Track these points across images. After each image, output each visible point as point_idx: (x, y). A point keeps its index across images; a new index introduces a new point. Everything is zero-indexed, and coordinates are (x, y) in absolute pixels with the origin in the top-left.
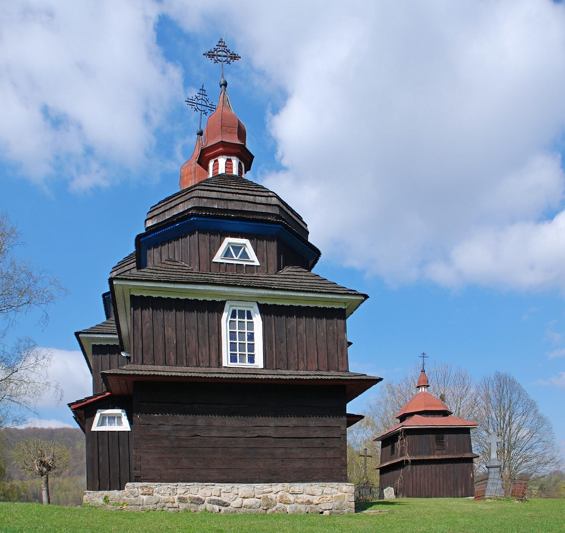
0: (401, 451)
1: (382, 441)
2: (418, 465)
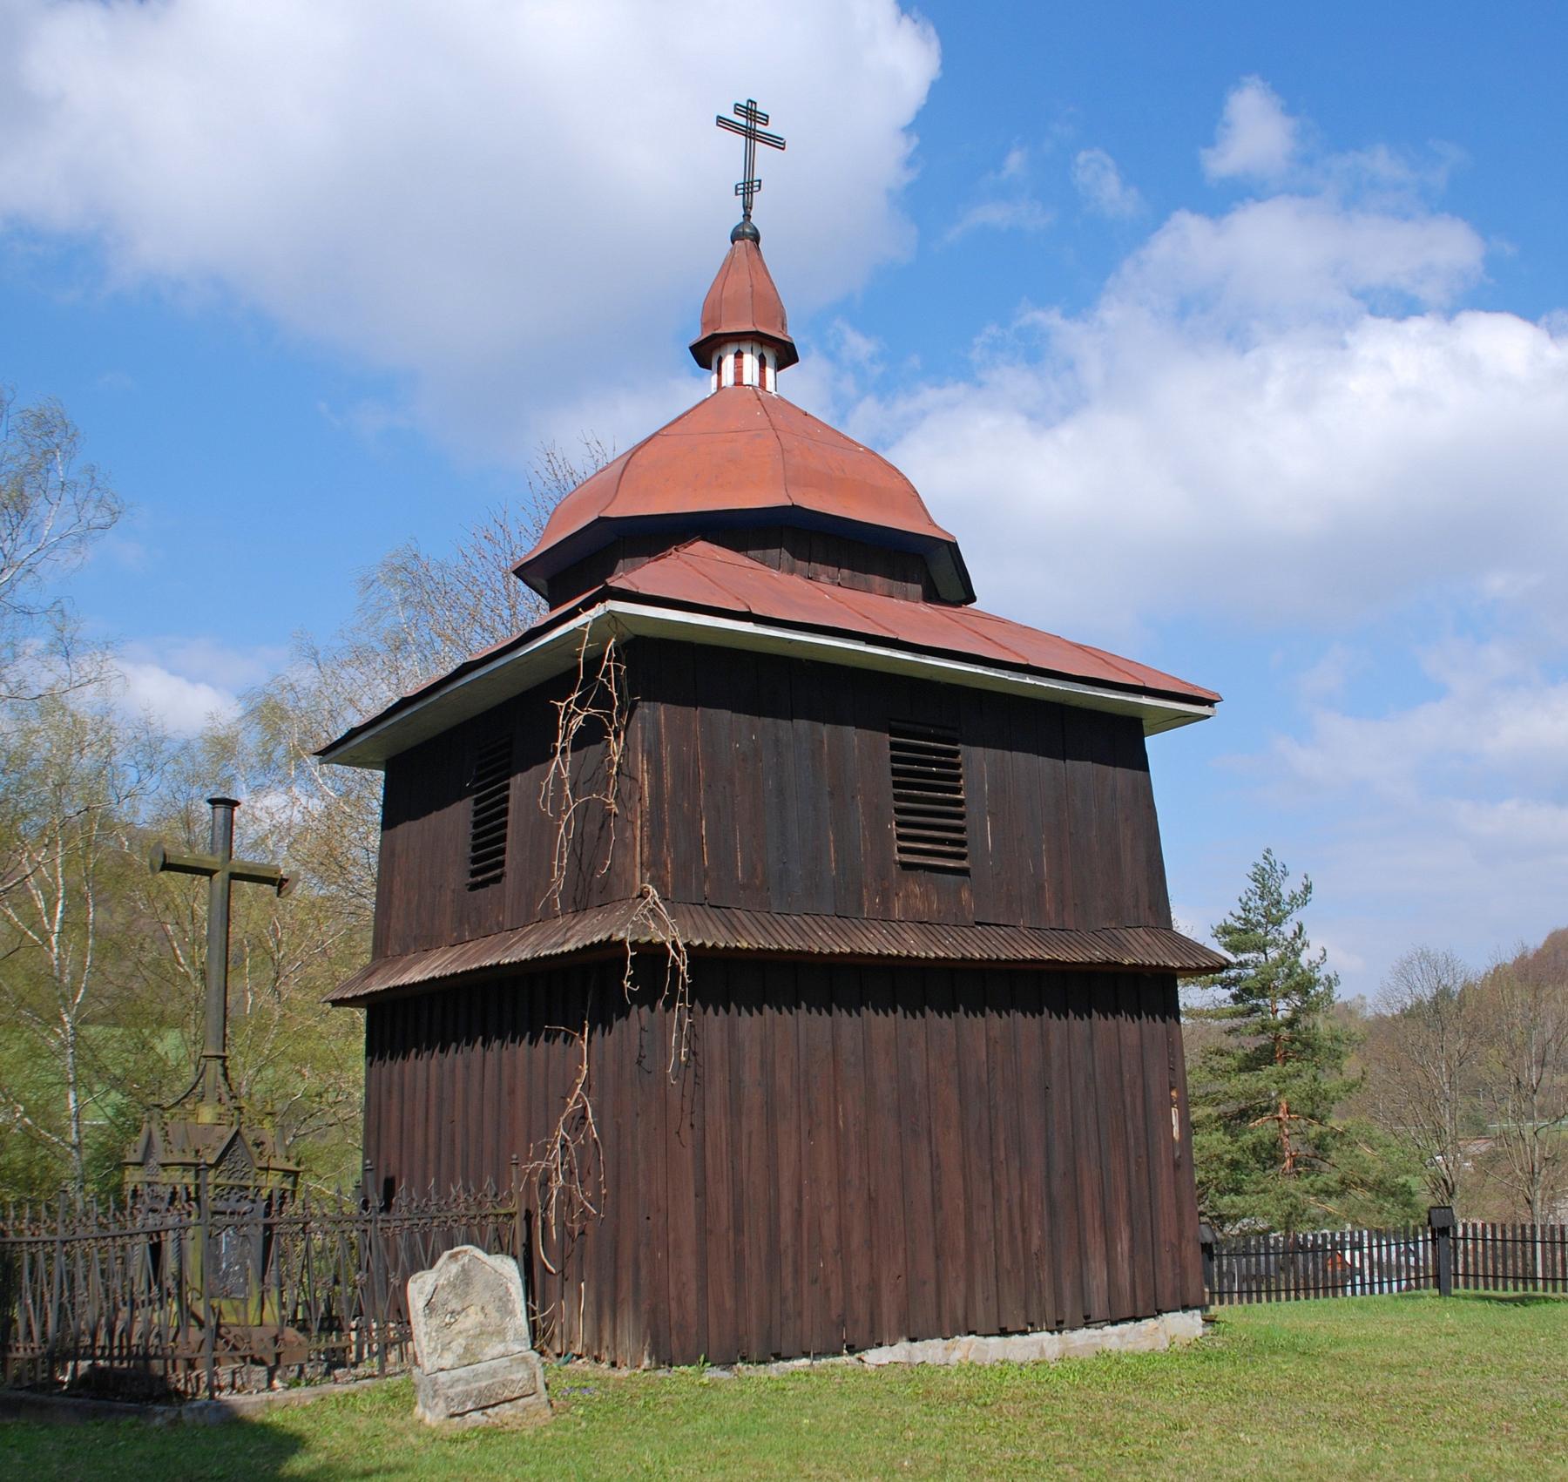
0: (578, 842)
2: (754, 1003)
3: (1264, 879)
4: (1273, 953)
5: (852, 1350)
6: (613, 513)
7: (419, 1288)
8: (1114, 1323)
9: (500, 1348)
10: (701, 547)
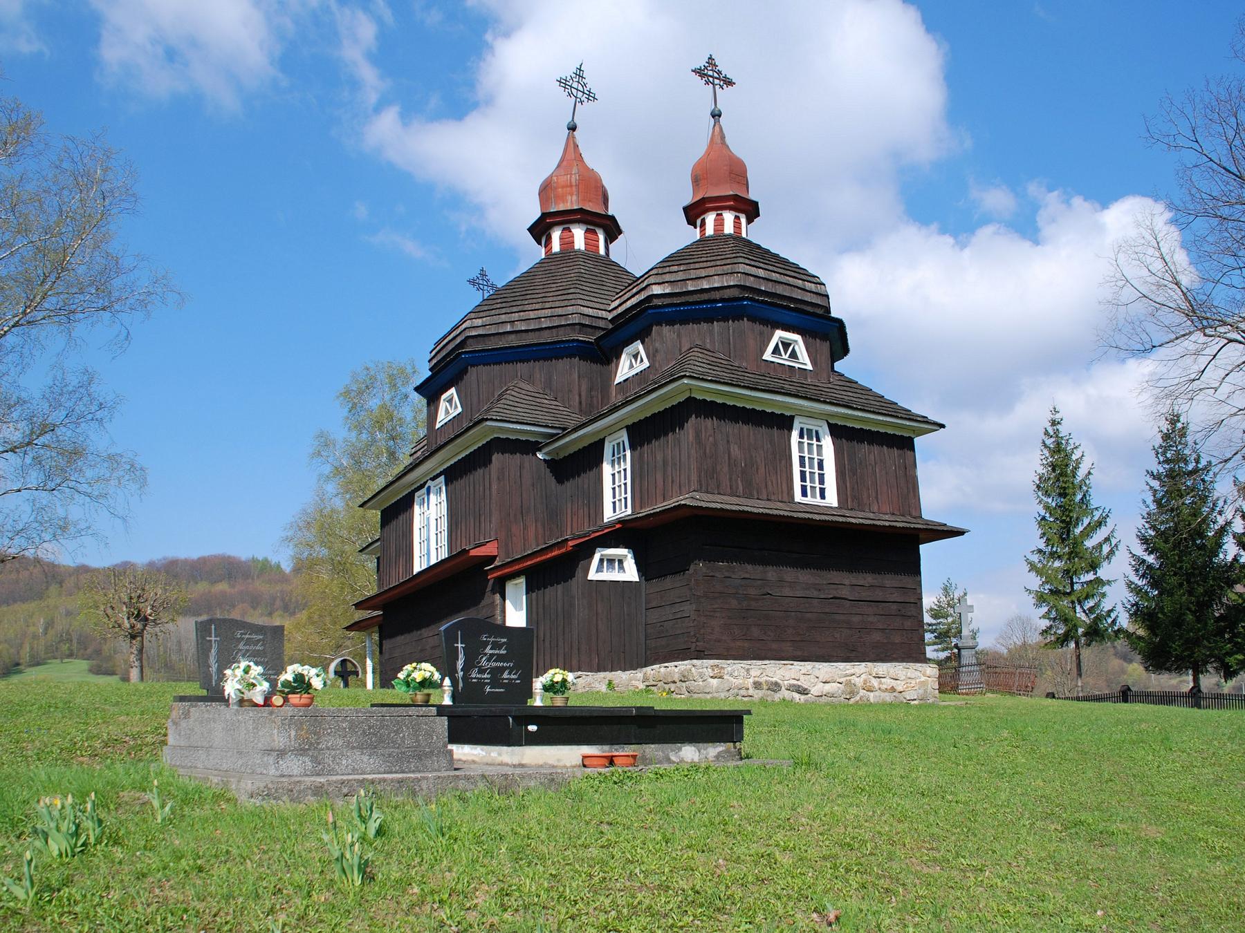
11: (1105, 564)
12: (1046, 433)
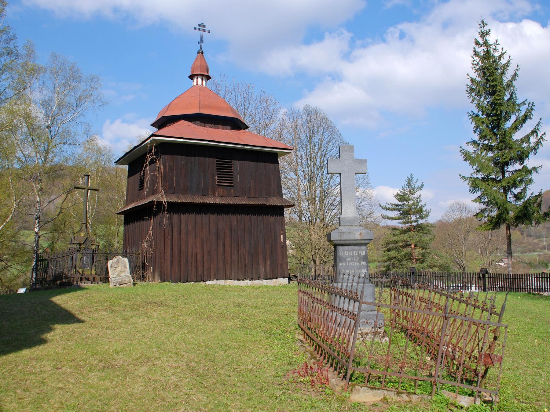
1: (130, 165)
2: (184, 213)
3: (409, 183)
4: (411, 202)
5: (203, 281)
6: (165, 115)
7: (110, 263)
8: (266, 279)
9: (124, 274)
10: (182, 122)
11: (531, 155)
12: (477, 43)
